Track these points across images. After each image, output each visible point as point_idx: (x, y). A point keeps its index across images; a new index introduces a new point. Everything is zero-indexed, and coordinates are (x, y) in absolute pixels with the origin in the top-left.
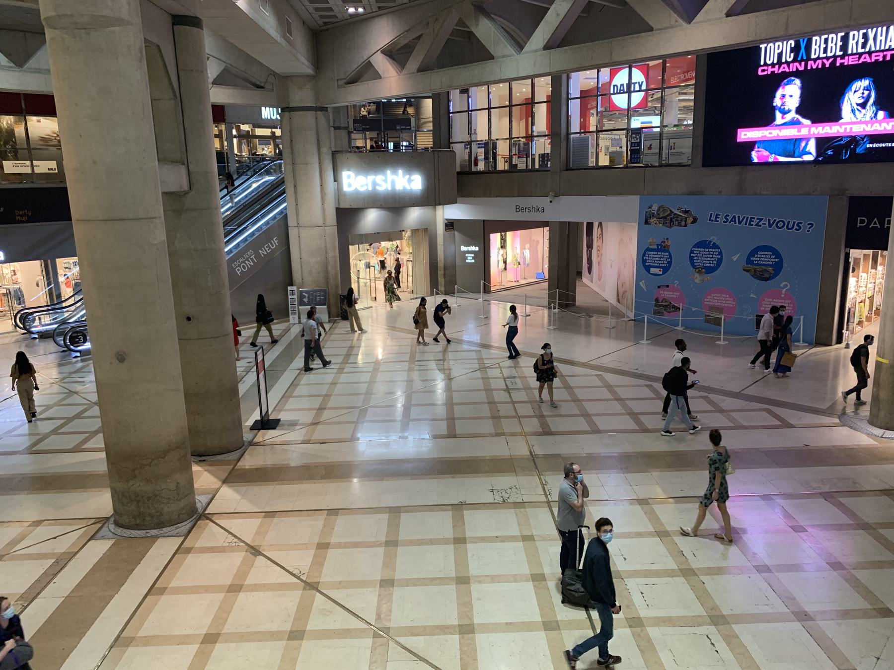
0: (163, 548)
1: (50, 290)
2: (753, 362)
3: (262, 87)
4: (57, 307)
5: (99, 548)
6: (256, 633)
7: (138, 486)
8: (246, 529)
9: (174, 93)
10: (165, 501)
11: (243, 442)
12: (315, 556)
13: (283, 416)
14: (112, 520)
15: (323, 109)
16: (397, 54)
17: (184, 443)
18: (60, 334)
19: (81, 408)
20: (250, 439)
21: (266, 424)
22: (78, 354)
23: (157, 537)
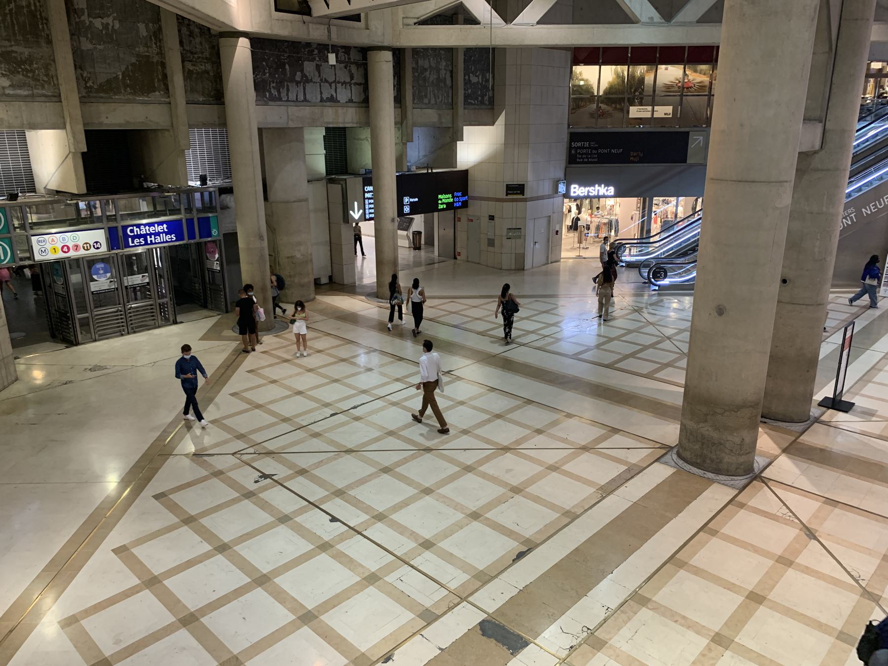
0: (717, 494)
1: (643, 222)
4: (644, 241)
5: (661, 472)
6: (802, 615)
7: (706, 430)
8: (806, 509)
9: (831, 49)
10: (727, 451)
11: (809, 416)
12: (879, 567)
13: (858, 401)
14: (675, 450)
17: (757, 404)
18: (645, 266)
19: (655, 339)
20: (816, 415)
21: (837, 404)
22: (657, 288)
23: (712, 481)
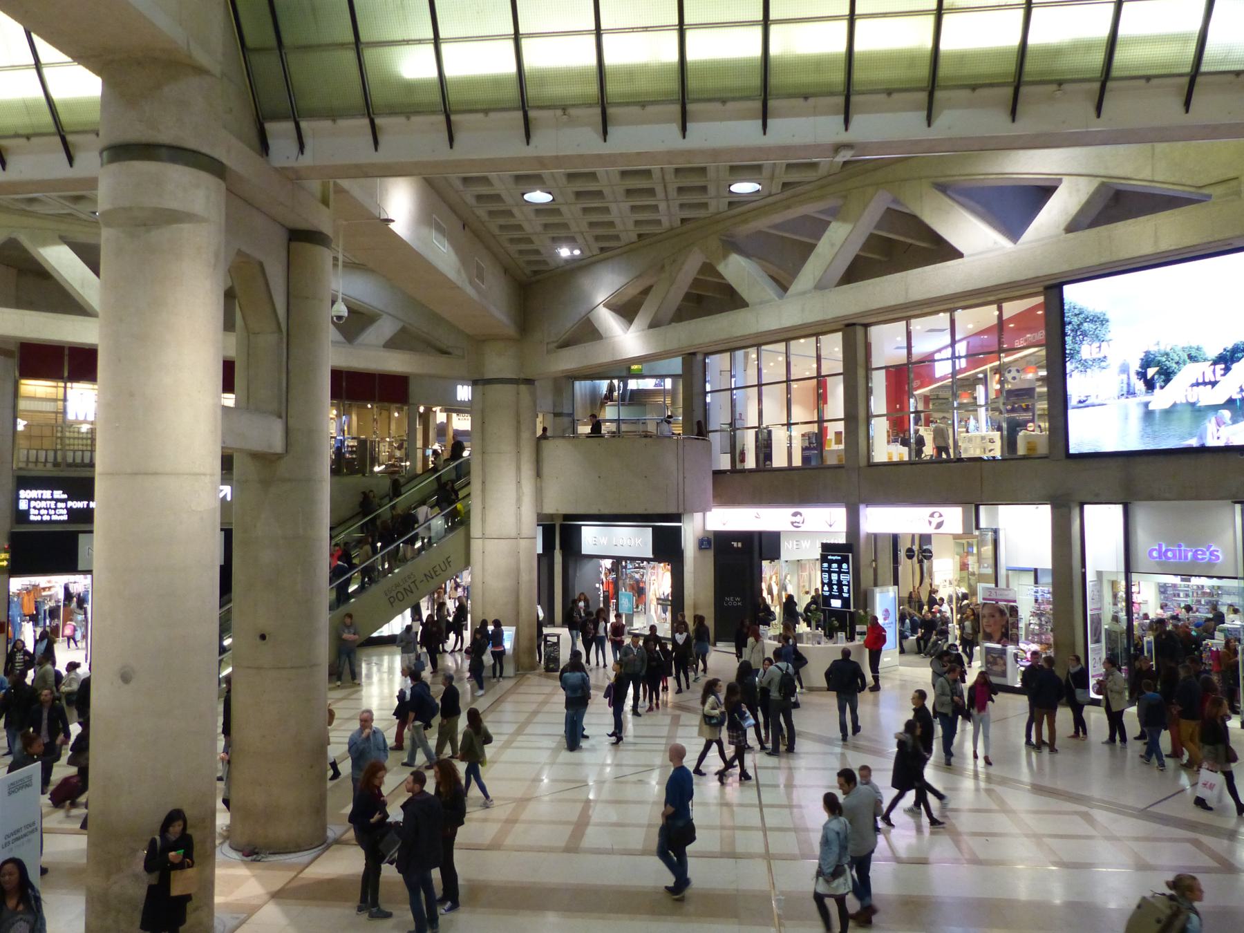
2: (574, 737)
3: (448, 353)
15: (529, 382)
16: (626, 310)
